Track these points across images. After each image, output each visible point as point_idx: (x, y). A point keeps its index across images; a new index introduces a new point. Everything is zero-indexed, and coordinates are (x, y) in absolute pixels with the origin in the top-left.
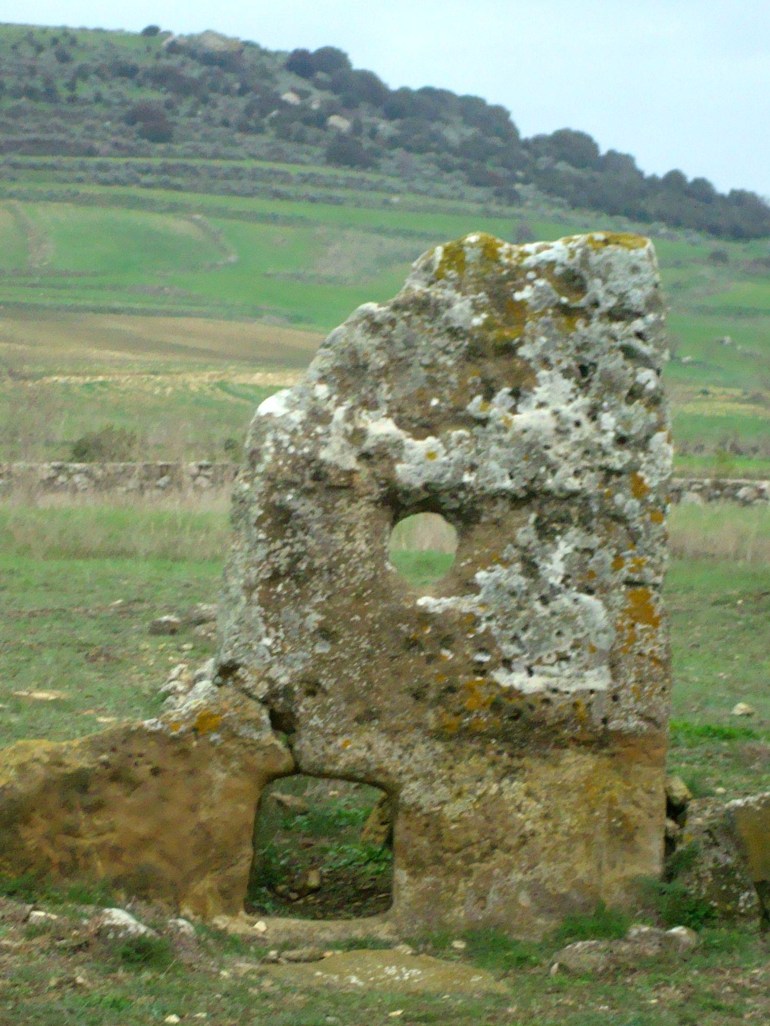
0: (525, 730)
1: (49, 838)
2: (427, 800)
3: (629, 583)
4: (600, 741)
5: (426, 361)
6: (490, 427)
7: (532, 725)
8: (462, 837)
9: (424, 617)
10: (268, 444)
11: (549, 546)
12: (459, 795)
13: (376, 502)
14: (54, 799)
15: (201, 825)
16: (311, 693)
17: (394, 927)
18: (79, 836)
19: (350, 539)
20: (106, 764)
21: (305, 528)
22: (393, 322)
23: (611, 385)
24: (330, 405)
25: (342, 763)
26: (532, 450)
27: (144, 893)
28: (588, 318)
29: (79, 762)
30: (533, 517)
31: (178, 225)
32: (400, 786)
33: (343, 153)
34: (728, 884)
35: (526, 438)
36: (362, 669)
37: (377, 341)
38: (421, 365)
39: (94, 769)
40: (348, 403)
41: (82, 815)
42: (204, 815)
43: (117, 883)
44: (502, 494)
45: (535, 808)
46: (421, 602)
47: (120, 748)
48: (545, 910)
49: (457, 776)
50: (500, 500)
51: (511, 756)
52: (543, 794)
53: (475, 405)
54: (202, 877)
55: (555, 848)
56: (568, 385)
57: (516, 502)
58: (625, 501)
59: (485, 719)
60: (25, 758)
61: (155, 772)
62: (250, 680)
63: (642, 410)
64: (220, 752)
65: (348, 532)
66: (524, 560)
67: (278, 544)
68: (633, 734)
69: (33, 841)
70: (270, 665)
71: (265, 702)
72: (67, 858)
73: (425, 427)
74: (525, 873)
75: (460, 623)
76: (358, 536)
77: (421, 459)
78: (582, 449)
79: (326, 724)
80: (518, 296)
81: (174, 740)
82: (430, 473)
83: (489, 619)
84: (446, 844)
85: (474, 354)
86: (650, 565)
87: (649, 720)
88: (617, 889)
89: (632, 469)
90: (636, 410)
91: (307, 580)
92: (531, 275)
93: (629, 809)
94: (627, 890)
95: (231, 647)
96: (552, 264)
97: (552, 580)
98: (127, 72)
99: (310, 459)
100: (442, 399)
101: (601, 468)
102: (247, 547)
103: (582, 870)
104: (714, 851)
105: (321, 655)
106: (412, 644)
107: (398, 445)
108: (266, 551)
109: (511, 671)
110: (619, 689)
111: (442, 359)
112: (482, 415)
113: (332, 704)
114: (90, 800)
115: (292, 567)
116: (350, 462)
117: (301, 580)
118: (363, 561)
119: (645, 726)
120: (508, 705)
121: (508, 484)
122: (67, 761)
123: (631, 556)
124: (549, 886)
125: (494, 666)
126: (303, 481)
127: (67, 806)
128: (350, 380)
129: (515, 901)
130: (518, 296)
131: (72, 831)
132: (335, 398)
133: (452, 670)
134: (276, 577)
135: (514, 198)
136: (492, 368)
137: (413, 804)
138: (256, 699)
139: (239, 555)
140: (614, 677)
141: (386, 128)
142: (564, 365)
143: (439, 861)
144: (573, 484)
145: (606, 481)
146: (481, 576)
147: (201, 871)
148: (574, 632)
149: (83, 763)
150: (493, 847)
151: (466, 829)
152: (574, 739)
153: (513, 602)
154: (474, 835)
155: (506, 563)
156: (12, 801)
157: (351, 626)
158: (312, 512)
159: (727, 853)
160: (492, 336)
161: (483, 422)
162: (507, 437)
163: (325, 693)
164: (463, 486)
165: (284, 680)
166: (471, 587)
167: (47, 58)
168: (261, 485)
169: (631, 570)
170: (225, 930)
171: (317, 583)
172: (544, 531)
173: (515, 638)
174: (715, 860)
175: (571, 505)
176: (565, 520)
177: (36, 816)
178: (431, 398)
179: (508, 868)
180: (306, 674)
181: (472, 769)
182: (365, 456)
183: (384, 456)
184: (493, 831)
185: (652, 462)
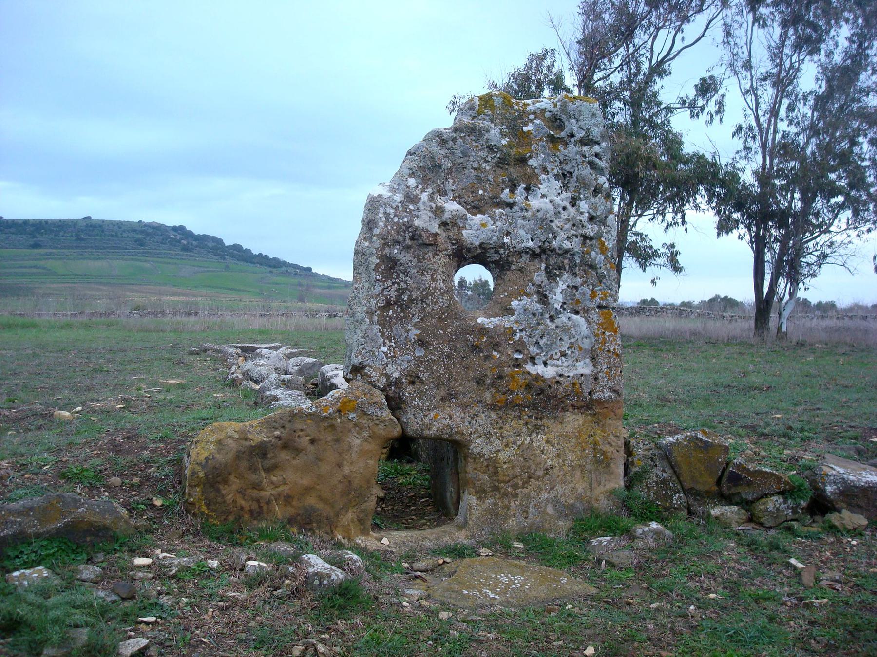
0: (545, 400)
1: (241, 492)
2: (487, 450)
3: (600, 307)
4: (589, 406)
5: (475, 165)
6: (516, 208)
7: (549, 398)
8: (511, 472)
9: (482, 330)
10: (381, 215)
11: (553, 284)
12: (507, 445)
13: (449, 255)
14: (244, 464)
15: (344, 477)
16: (412, 383)
17: (469, 534)
18: (262, 489)
19: (434, 280)
20: (279, 438)
21: (406, 273)
22: (454, 140)
23: (583, 184)
24: (418, 192)
25: (434, 429)
26: (544, 223)
27: (308, 527)
28: (566, 144)
29: (260, 437)
30: (543, 266)
31: (147, 265)
32: (471, 442)
33: (185, 249)
34: (666, 490)
35: (540, 215)
36: (445, 365)
37: (443, 152)
38: (473, 168)
39: (271, 441)
40: (430, 190)
41: (263, 474)
42: (346, 470)
43: (291, 521)
44: (526, 251)
45: (552, 450)
46: (479, 320)
47: (288, 425)
48: (561, 515)
49: (505, 433)
50: (523, 255)
51: (536, 418)
52: (556, 441)
53: (505, 194)
54: (347, 512)
55: (564, 475)
56: (558, 184)
57: (534, 255)
58: (596, 256)
59: (521, 396)
60: (222, 436)
61: (312, 441)
62: (375, 376)
63: (603, 200)
64: (356, 425)
65: (432, 276)
66: (538, 292)
67: (390, 282)
68: (607, 401)
69: (230, 497)
70: (387, 365)
71: (383, 390)
72: (255, 506)
73: (476, 209)
74: (549, 493)
75: (504, 334)
76: (439, 278)
77: (478, 228)
78: (571, 223)
79: (423, 403)
80: (525, 129)
81: (326, 418)
82: (484, 237)
83: (521, 331)
84: (501, 478)
85: (503, 162)
86: (611, 295)
87: (615, 391)
88: (602, 497)
89: (599, 236)
90: (599, 200)
91: (408, 307)
92: (531, 117)
93: (607, 448)
94: (608, 498)
95: (360, 353)
96: (544, 110)
97: (556, 306)
98: (135, 231)
99: (408, 226)
100: (484, 191)
101: (582, 235)
102: (367, 285)
103: (581, 487)
104: (655, 470)
105: (419, 357)
106: (475, 348)
107: (463, 218)
108: (380, 289)
109: (534, 364)
110: (598, 373)
111: (484, 165)
112: (510, 200)
113: (427, 390)
114: (268, 463)
115: (399, 297)
116: (435, 228)
117: (405, 307)
118: (442, 294)
119: (613, 395)
120: (535, 384)
121: (531, 244)
122: (251, 436)
123: (600, 290)
124: (563, 499)
125: (525, 362)
126: (405, 240)
127: (253, 469)
128: (430, 175)
129: (544, 512)
130: (525, 129)
131: (257, 486)
132: (420, 187)
133: (500, 365)
134: (388, 304)
135: (224, 259)
136: (514, 171)
137: (479, 454)
138: (379, 388)
139: (361, 291)
140: (595, 366)
141: (195, 243)
142: (555, 172)
143: (496, 489)
144: (567, 245)
145: (584, 243)
146: (514, 303)
147: (346, 508)
148: (570, 338)
149: (262, 437)
150: (530, 478)
151: (513, 467)
152: (572, 406)
153: (534, 321)
154: (518, 470)
155: (529, 295)
156: (215, 468)
157: (437, 337)
158: (411, 261)
159: (664, 471)
160: (513, 152)
161: (511, 205)
162: (528, 214)
163: (422, 382)
164: (503, 245)
165: (396, 375)
166: (509, 311)
167: (116, 227)
168: (377, 243)
169: (602, 299)
170: (366, 547)
171: (414, 309)
172: (551, 276)
173: (537, 343)
174: (657, 476)
175: (565, 258)
176: (561, 268)
177: (232, 477)
178: (478, 189)
179: (539, 490)
180: (409, 371)
181: (514, 428)
182: (444, 224)
183: (455, 225)
184: (529, 468)
185: (609, 232)
